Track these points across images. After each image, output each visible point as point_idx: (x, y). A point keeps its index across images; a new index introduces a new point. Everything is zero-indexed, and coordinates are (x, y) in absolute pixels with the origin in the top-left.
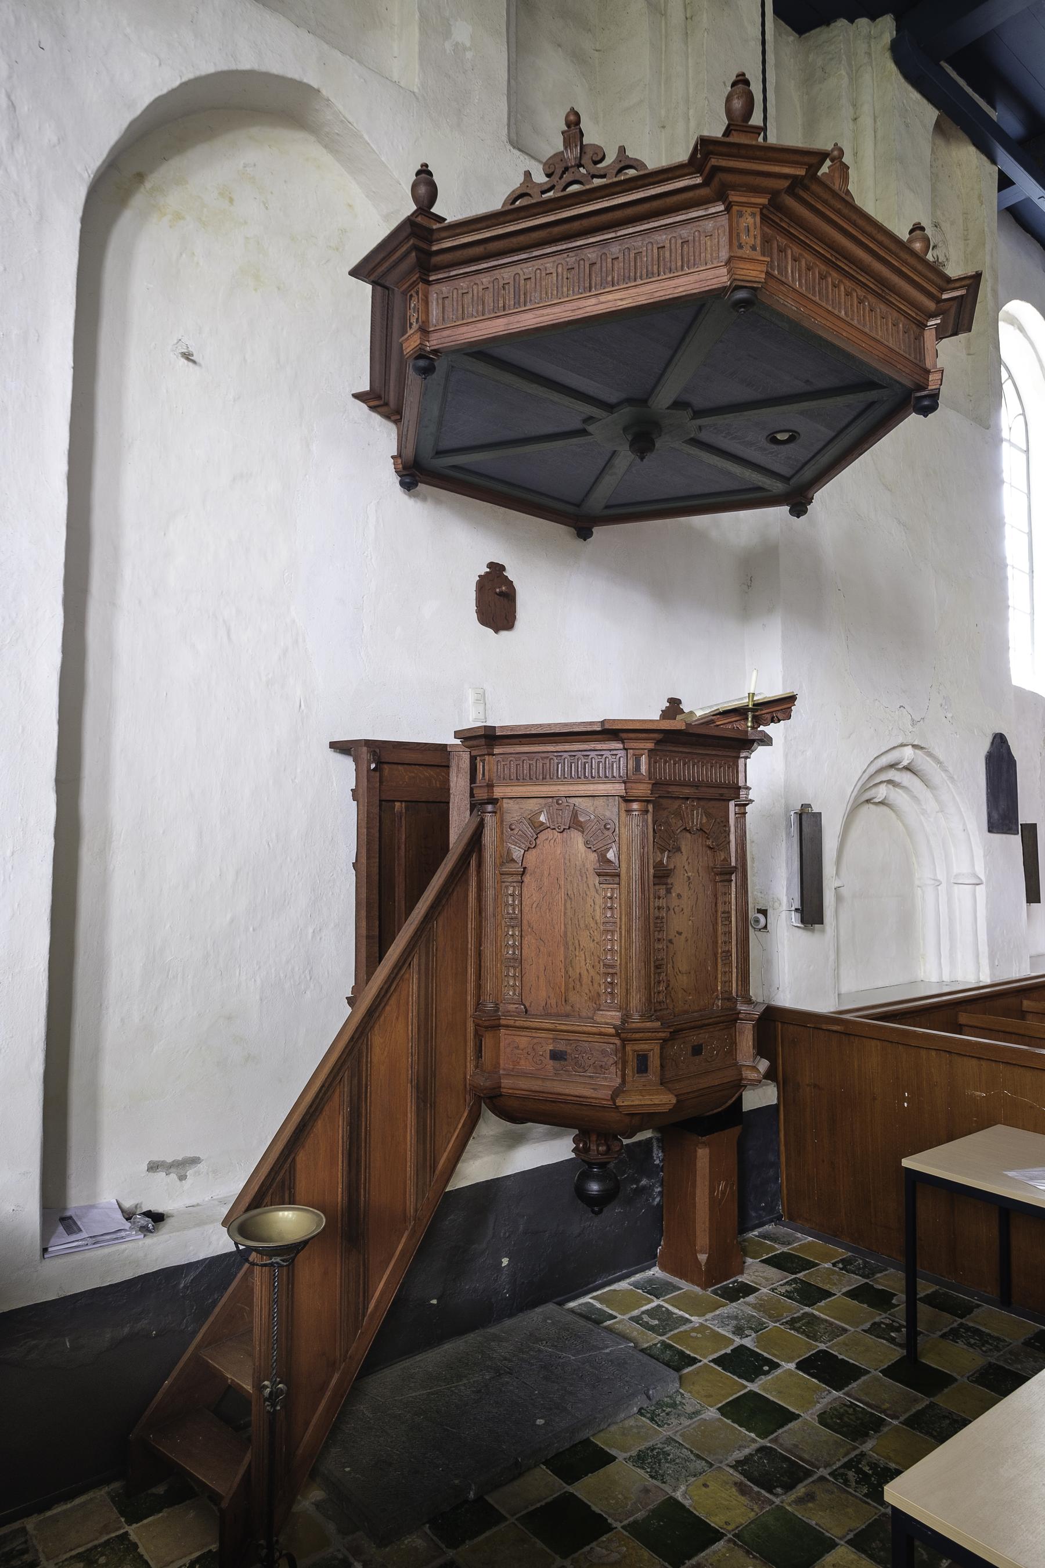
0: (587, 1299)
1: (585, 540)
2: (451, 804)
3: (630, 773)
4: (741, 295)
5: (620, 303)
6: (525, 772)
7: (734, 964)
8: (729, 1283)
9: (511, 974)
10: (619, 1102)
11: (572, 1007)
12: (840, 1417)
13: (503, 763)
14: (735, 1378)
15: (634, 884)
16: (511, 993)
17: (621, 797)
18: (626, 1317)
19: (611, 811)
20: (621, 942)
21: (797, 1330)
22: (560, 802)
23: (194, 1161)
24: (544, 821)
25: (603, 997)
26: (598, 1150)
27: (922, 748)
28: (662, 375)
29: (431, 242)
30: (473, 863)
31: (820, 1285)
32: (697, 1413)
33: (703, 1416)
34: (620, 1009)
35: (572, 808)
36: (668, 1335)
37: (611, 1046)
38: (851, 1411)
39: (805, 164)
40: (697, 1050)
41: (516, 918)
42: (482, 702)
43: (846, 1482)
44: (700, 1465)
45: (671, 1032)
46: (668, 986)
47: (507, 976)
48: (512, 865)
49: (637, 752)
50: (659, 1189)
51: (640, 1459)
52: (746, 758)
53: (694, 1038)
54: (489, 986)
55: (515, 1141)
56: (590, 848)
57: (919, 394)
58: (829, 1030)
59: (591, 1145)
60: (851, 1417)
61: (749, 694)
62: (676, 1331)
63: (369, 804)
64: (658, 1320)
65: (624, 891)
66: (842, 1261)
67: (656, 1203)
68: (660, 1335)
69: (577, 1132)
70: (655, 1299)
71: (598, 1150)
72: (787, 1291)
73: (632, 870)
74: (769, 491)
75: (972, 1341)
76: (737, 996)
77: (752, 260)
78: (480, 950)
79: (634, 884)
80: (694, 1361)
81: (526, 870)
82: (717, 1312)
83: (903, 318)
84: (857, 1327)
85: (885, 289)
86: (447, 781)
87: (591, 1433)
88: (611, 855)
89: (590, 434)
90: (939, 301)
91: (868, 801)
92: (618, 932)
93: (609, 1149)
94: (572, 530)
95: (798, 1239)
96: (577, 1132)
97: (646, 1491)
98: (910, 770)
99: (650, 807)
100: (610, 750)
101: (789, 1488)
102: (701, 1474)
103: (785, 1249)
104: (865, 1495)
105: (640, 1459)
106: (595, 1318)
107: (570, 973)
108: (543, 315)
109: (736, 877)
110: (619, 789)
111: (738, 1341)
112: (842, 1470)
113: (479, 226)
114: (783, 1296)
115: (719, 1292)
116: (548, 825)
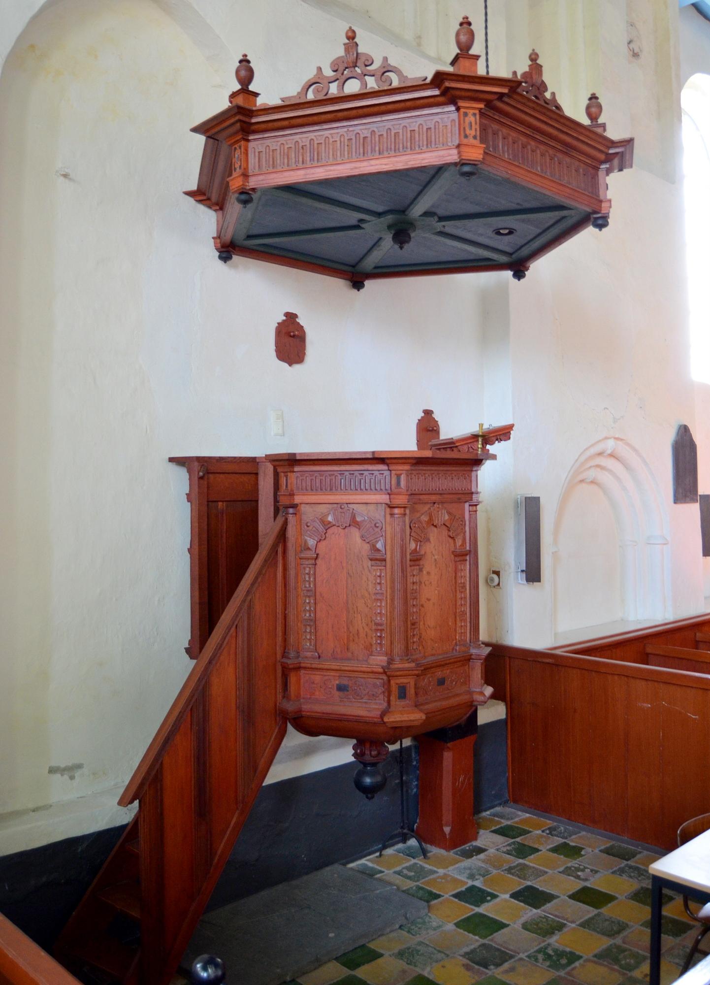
0: (363, 861)
1: (358, 290)
2: (259, 502)
3: (393, 487)
4: (466, 169)
5: (384, 167)
6: (317, 485)
7: (468, 620)
8: (466, 847)
9: (308, 631)
10: (386, 719)
11: (352, 653)
12: (537, 924)
13: (301, 478)
14: (467, 905)
15: (396, 566)
16: (308, 644)
17: (387, 504)
18: (391, 871)
19: (379, 514)
20: (387, 608)
21: (513, 874)
22: (343, 507)
23: (79, 766)
24: (331, 521)
25: (374, 646)
26: (371, 754)
27: (621, 440)
28: (415, 199)
29: (251, 117)
30: (280, 550)
31: (532, 845)
32: (440, 927)
33: (444, 929)
34: (386, 654)
35: (351, 511)
36: (421, 882)
37: (380, 681)
38: (545, 920)
39: (508, 86)
40: (441, 682)
41: (311, 590)
42: (281, 420)
43: (536, 960)
44: (440, 956)
45: (422, 670)
46: (420, 637)
47: (305, 632)
48: (308, 552)
49: (398, 472)
50: (416, 783)
51: (401, 954)
52: (476, 471)
53: (439, 674)
54: (292, 639)
55: (308, 752)
56: (365, 540)
57: (595, 216)
58: (543, 663)
59: (366, 751)
60: (544, 923)
61: (479, 424)
62: (427, 879)
63: (200, 504)
64: (414, 872)
65: (388, 570)
66: (549, 829)
67: (413, 793)
68: (416, 882)
69: (354, 741)
70: (412, 859)
71: (371, 754)
72: (507, 850)
73: (392, 556)
74: (497, 261)
75: (632, 874)
76: (470, 642)
77: (473, 146)
78: (285, 614)
79: (396, 566)
80: (438, 896)
81: (318, 556)
82: (457, 866)
83: (582, 165)
84: (554, 870)
85: (569, 149)
86: (256, 484)
87: (367, 940)
88: (379, 545)
89: (363, 228)
90: (607, 154)
91: (582, 481)
92: (385, 601)
93: (379, 753)
94: (348, 283)
95: (519, 816)
96: (354, 741)
97: (404, 972)
98: (614, 457)
99: (408, 511)
100: (379, 471)
101: (498, 965)
102: (440, 960)
103: (509, 823)
104: (549, 967)
105: (401, 954)
106: (370, 874)
107: (351, 629)
108: (331, 171)
109: (470, 557)
110: (385, 498)
111: (470, 883)
112: (534, 954)
113: (286, 109)
114: (505, 853)
115: (459, 853)
116: (334, 523)
